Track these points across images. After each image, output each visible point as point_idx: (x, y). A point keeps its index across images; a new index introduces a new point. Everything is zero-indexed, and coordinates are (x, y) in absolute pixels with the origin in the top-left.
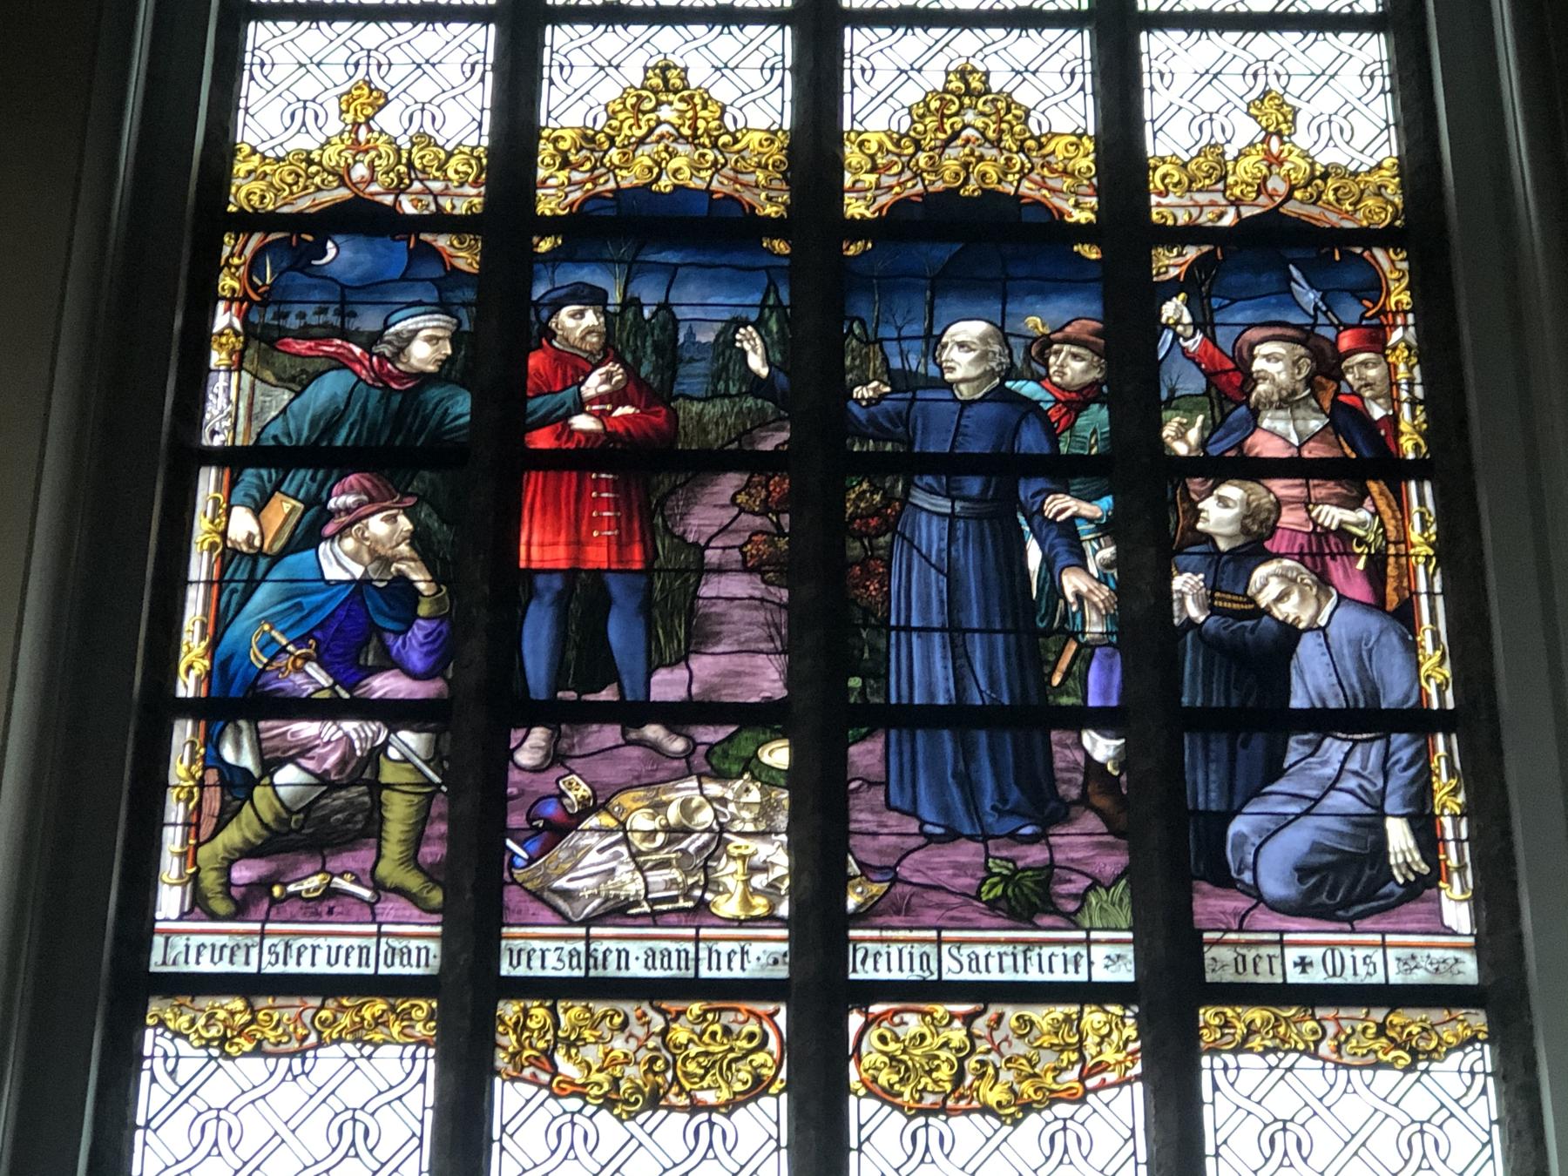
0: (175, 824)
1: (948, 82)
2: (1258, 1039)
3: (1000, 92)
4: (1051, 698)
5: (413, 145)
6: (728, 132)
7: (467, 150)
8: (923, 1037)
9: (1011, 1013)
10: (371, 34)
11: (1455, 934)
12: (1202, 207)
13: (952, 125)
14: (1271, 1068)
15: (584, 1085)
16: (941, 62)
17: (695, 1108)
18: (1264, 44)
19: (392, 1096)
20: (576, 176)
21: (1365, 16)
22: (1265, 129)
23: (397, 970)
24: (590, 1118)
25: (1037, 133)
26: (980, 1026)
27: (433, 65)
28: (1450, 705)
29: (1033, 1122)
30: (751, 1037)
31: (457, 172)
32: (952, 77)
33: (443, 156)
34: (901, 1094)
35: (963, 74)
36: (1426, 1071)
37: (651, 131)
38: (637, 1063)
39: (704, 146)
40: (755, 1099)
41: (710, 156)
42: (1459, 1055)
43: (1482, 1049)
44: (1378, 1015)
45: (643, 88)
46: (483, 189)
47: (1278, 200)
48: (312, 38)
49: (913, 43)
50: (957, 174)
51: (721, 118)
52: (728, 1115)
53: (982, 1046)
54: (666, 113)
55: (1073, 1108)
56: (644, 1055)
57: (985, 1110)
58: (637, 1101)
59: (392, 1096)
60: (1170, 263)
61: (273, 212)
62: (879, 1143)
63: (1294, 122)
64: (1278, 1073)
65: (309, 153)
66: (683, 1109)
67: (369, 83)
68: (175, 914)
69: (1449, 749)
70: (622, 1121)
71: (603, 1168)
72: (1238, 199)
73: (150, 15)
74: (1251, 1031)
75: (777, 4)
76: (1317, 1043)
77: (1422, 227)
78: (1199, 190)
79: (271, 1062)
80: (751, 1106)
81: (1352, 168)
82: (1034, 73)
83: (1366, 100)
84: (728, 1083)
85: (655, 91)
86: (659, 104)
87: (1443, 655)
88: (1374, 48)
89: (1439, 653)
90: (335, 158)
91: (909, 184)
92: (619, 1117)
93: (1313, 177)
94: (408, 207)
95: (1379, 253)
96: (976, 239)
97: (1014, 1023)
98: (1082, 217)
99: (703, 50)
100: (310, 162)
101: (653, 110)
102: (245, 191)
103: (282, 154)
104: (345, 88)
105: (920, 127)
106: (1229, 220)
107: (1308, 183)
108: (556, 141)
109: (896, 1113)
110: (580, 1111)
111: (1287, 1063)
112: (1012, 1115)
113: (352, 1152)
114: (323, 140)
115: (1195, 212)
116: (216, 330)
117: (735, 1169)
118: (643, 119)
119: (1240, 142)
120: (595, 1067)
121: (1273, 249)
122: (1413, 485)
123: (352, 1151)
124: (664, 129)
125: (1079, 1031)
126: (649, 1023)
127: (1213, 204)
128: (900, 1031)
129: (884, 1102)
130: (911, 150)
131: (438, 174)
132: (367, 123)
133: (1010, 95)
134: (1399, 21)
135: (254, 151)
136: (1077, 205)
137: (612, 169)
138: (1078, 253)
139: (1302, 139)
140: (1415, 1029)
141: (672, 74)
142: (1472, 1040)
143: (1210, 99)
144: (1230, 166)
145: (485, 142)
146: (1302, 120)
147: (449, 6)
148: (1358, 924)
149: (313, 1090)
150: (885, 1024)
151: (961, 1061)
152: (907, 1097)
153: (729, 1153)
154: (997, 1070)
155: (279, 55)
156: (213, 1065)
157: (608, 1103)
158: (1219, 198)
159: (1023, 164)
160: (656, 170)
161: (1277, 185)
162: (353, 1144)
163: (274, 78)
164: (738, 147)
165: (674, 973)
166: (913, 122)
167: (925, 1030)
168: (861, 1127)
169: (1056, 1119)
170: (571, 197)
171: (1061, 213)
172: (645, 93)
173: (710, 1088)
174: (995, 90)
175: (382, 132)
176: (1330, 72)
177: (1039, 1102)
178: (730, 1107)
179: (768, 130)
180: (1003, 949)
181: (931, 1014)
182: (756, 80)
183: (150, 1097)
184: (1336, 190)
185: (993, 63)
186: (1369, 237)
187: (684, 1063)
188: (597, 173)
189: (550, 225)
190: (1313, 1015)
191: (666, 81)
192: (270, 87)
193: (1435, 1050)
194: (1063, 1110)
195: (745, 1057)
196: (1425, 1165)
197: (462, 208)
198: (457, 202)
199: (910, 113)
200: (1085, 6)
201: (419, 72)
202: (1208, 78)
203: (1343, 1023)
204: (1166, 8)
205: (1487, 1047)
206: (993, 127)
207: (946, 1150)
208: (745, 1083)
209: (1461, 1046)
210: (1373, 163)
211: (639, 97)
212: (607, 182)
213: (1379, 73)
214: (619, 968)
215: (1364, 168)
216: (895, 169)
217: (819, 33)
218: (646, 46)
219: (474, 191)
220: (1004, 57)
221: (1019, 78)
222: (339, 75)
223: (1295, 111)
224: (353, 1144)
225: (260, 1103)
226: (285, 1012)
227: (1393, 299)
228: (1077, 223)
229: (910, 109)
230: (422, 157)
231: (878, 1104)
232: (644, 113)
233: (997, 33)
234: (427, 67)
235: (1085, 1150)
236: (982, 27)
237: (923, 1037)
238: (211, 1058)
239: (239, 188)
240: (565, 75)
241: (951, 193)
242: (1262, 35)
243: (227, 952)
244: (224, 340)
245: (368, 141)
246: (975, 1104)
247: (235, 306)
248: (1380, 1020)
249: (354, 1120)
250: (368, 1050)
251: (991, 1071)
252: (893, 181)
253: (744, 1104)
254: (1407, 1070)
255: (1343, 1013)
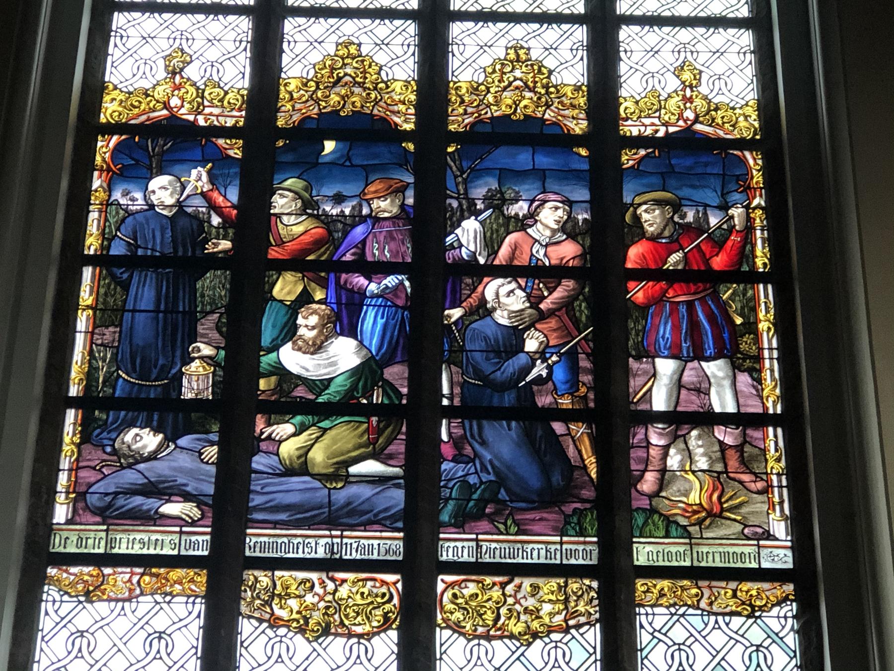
0: (64, 470)
1: (507, 54)
2: (665, 599)
3: (367, 55)
4: (404, 402)
5: (206, 86)
6: (383, 81)
7: (236, 90)
8: (477, 595)
9: (527, 583)
10: (183, 21)
11: (777, 539)
12: (646, 126)
13: (337, 74)
14: (672, 615)
15: (288, 621)
16: (503, 42)
17: (350, 635)
18: (684, 34)
19: (181, 624)
20: (470, 110)
21: (579, 15)
22: (683, 83)
23: (573, 561)
24: (291, 639)
25: (385, 79)
26: (510, 589)
27: (320, 43)
28: (779, 411)
29: (538, 644)
30: (384, 595)
31: (229, 103)
32: (509, 51)
33: (222, 93)
34: (464, 627)
35: (516, 49)
36: (760, 617)
37: (510, 84)
38: (318, 609)
39: (369, 89)
40: (385, 631)
41: (373, 96)
42: (778, 608)
43: (791, 605)
44: (733, 585)
45: (336, 55)
46: (243, 113)
47: (689, 123)
48: (150, 22)
49: (487, 32)
50: (339, 103)
51: (379, 73)
52: (369, 640)
53: (510, 601)
54: (518, 73)
55: (560, 636)
56: (322, 605)
57: (512, 637)
58: (318, 630)
59: (181, 624)
60: (628, 159)
61: (126, 123)
62: (453, 655)
63: (700, 80)
64: (675, 618)
65: (147, 90)
66: (341, 635)
67: (182, 50)
68: (63, 521)
69: (776, 436)
70: (310, 642)
71: (298, 667)
72: (667, 122)
73: (49, 9)
74: (662, 595)
75: (246, 3)
76: (698, 601)
77: (768, 140)
78: (645, 117)
79: (113, 604)
80: (382, 635)
81: (731, 105)
82: (555, 49)
83: (741, 67)
84: (370, 622)
85: (512, 62)
86: (344, 65)
87: (776, 384)
88: (244, 24)
89: (773, 383)
90: (161, 93)
91: (483, 112)
92: (307, 639)
93: (709, 111)
94: (201, 121)
95: (747, 154)
96: (517, 141)
97: (529, 589)
98: (409, 127)
99: (369, 33)
100: (148, 95)
101: (511, 71)
102: (111, 110)
103: (131, 89)
104: (168, 53)
105: (490, 80)
106: (661, 134)
107: (707, 113)
108: (457, 89)
109: (461, 638)
110: (285, 636)
111: (681, 612)
112: (527, 639)
113: (358, 661)
114: (155, 83)
115: (642, 129)
116: (93, 188)
117: (294, 668)
118: (505, 78)
119: (670, 89)
120: (294, 612)
121: (690, 154)
122: (761, 286)
123: (80, 656)
124: (348, 78)
125: (565, 593)
126: (325, 587)
127: (653, 124)
128: (465, 591)
129: (454, 631)
130: (313, 89)
131: (219, 104)
132: (180, 73)
133: (541, 62)
134: (757, 22)
135: (115, 88)
136: (405, 121)
137: (488, 106)
138: (404, 148)
139: (704, 89)
140: (754, 593)
141: (521, 52)
142: (786, 599)
143: (653, 65)
144: (663, 103)
145: (247, 85)
146: (705, 77)
147: (163, 4)
148: (367, 527)
149: (136, 620)
150: (456, 587)
151: (498, 609)
152: (467, 628)
153: (290, 659)
154: (519, 613)
155: (131, 32)
156: (81, 606)
157: (302, 631)
158: (656, 121)
159: (376, 98)
160: (342, 102)
161: (689, 115)
162: (358, 657)
163: (128, 45)
164: (389, 90)
165: (535, 561)
166: (486, 77)
167: (479, 592)
168: (441, 645)
169: (552, 641)
170: (466, 121)
171: (396, 125)
172: (506, 62)
173: (360, 624)
174: (533, 59)
175: (189, 79)
176: (655, 49)
177: (542, 632)
178: (369, 636)
179: (575, 85)
180: (540, 546)
181: (482, 582)
182: (568, 56)
183: (46, 623)
184: (723, 118)
185: (532, 43)
186: (742, 144)
187: (345, 610)
188: (481, 108)
189: (455, 137)
190: (697, 584)
191: (518, 55)
192: (126, 50)
193: (765, 605)
194: (555, 636)
195: (379, 607)
196: (556, 665)
197: (230, 123)
198: (228, 119)
199: (314, 67)
200: (252, 3)
201: (312, 47)
202: (651, 53)
203: (714, 590)
204: (296, 5)
205: (794, 604)
206: (531, 80)
207: (90, 650)
208: (379, 622)
209: (779, 603)
210: (743, 103)
211: (503, 64)
212: (486, 113)
213: (413, 43)
214: (546, 558)
215: (738, 106)
216: (475, 104)
217: (433, 24)
218: (506, 35)
219: (238, 114)
220: (540, 41)
221: (547, 52)
222: (164, 44)
223: (701, 72)
224: (358, 657)
225: (184, 629)
226: (121, 577)
227: (755, 180)
228: (405, 130)
229: (484, 68)
230: (211, 93)
231: (451, 632)
232: (336, 69)
233: (201, 17)
234: (316, 44)
235: (369, 656)
236: (693, 26)
237: (477, 595)
238: (157, 603)
239: (106, 109)
240: (124, 41)
241: (336, 113)
242: (683, 29)
243: (301, 547)
244: (97, 194)
245: (181, 84)
246: (506, 633)
247: (104, 175)
248: (734, 588)
249: (680, 649)
250: (168, 598)
251: (515, 614)
252: (474, 110)
253: (378, 633)
254: (748, 617)
255: (714, 583)
